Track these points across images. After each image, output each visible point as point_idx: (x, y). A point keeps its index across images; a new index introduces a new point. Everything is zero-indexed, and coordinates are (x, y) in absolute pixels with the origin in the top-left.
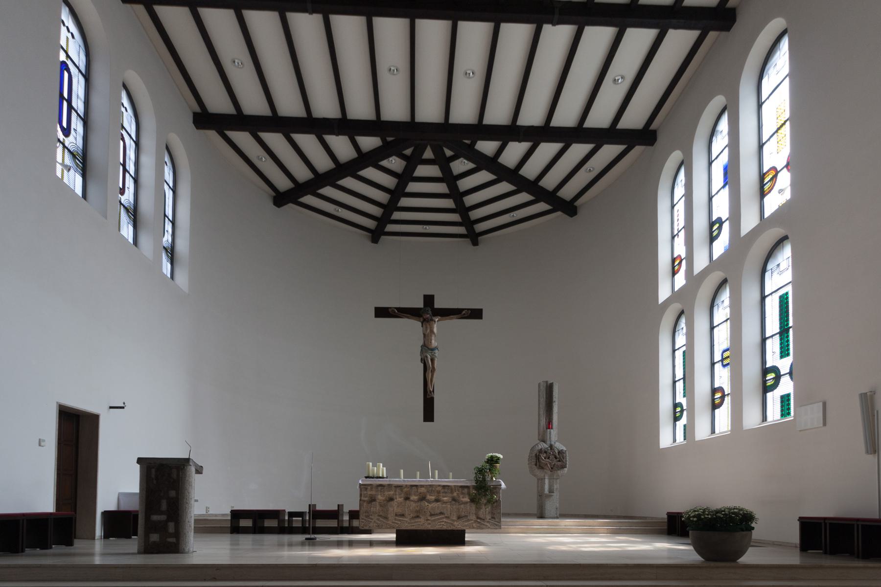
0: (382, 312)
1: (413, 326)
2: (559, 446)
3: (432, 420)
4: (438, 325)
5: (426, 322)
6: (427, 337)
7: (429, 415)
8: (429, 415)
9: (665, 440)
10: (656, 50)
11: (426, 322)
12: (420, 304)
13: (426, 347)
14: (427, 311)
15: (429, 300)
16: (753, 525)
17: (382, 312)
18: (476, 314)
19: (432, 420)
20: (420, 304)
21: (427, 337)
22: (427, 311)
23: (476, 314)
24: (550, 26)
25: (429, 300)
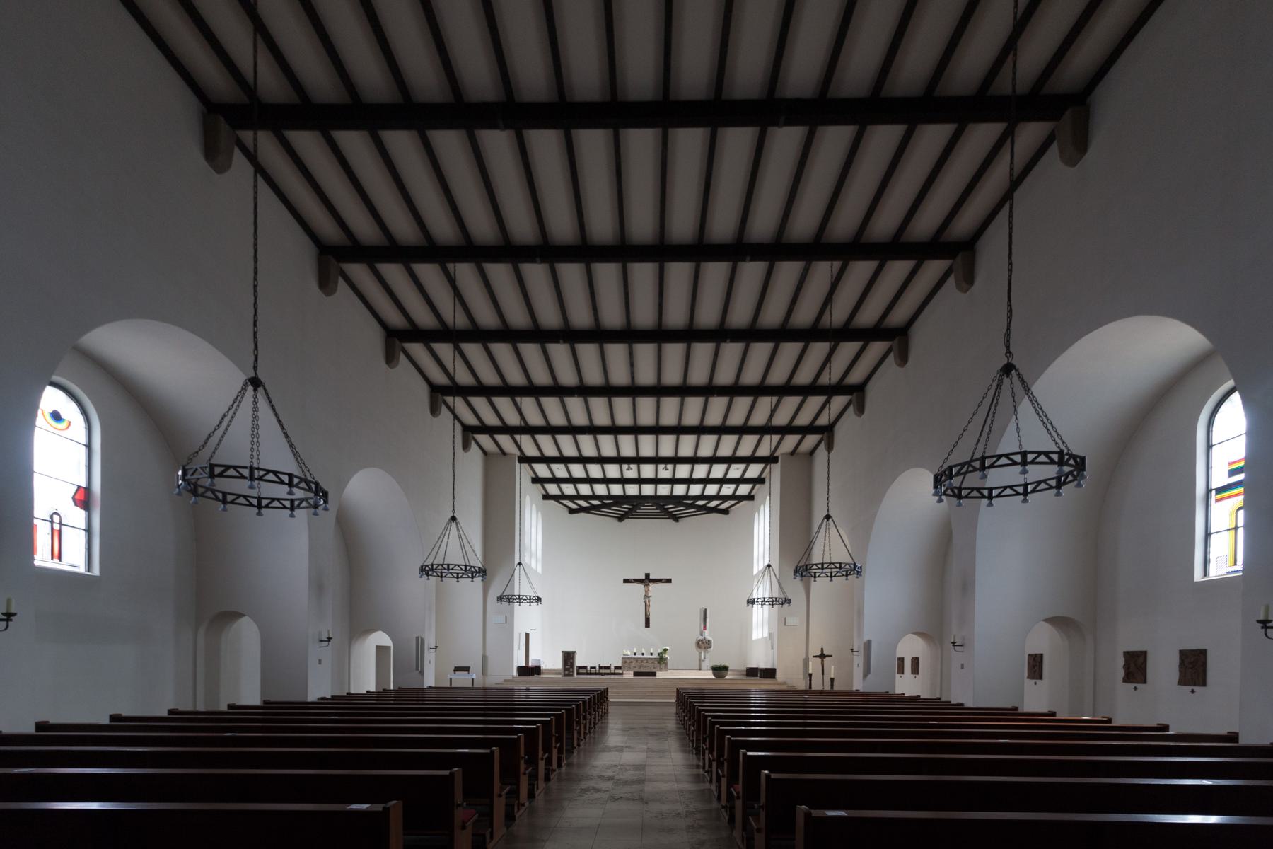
0: (626, 581)
1: (641, 587)
2: (708, 638)
3: (1184, 655)
4: (652, 586)
5: (647, 585)
6: (647, 591)
7: (647, 625)
8: (647, 625)
9: (754, 638)
10: (726, 52)
11: (647, 585)
12: (643, 577)
13: (646, 596)
14: (647, 580)
15: (647, 575)
16: (551, 662)
17: (626, 581)
18: (669, 581)
19: (1184, 655)
20: (643, 577)
21: (647, 591)
22: (647, 580)
23: (669, 581)
24: (776, 128)
25: (647, 575)
